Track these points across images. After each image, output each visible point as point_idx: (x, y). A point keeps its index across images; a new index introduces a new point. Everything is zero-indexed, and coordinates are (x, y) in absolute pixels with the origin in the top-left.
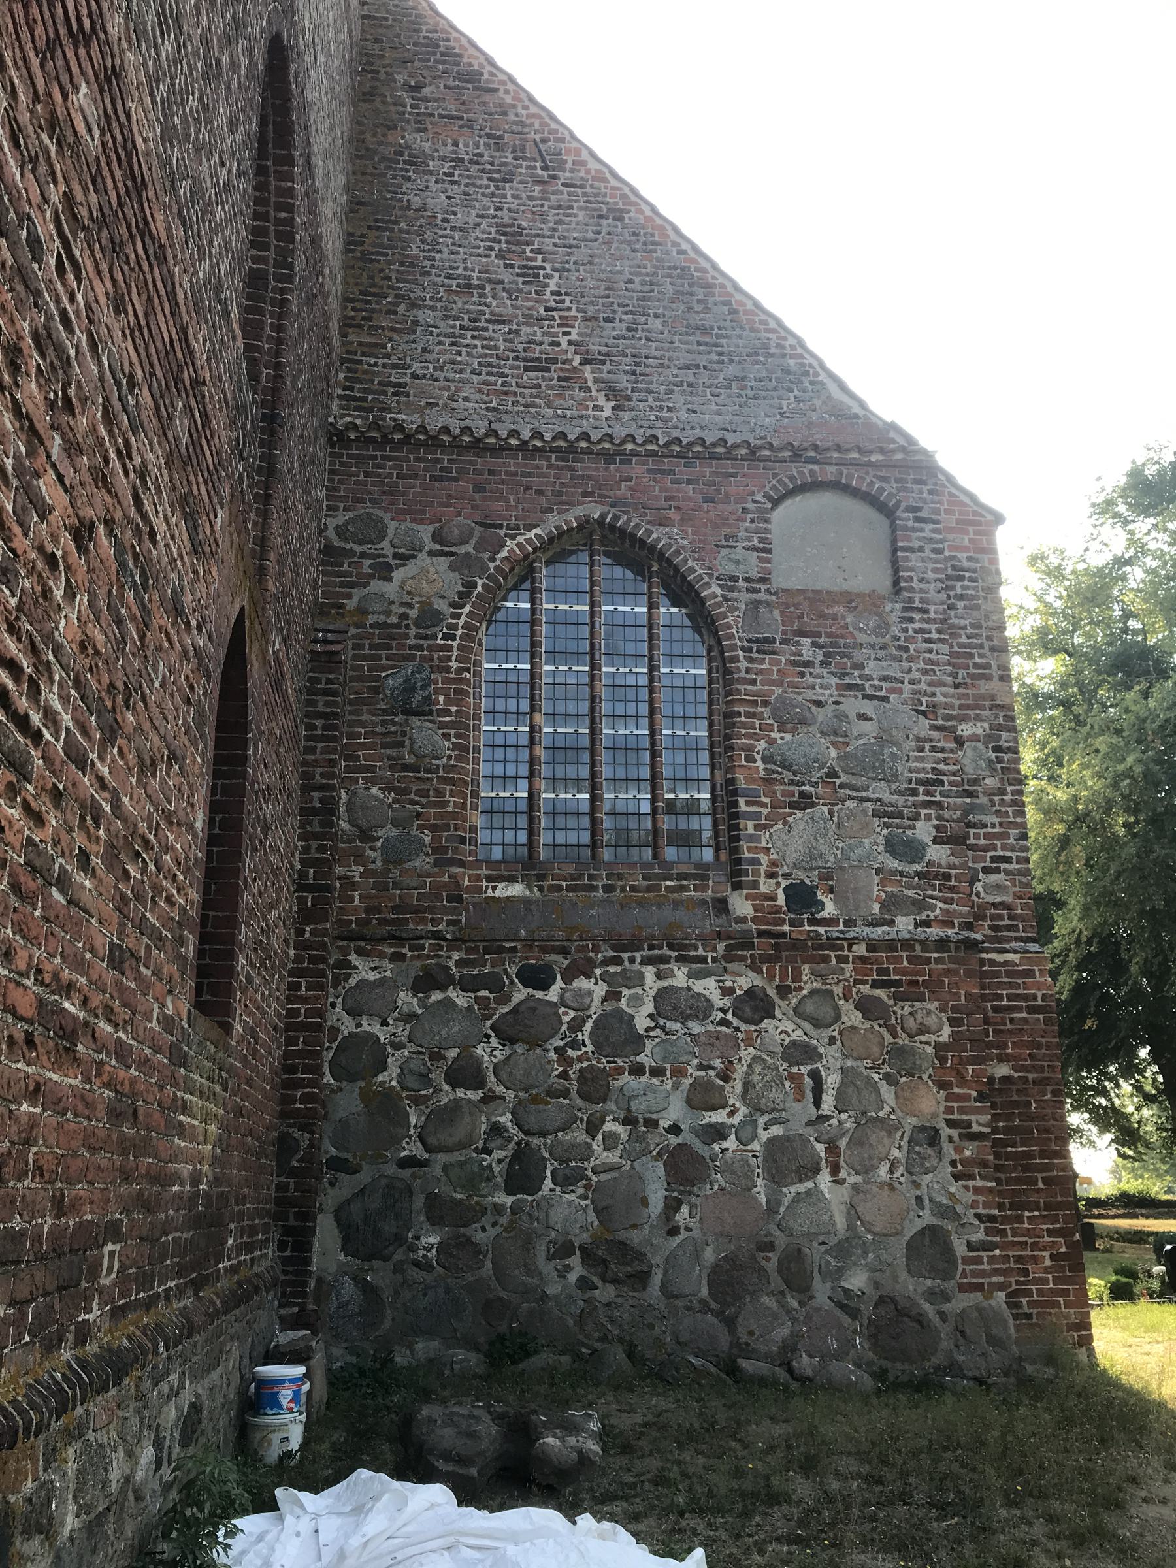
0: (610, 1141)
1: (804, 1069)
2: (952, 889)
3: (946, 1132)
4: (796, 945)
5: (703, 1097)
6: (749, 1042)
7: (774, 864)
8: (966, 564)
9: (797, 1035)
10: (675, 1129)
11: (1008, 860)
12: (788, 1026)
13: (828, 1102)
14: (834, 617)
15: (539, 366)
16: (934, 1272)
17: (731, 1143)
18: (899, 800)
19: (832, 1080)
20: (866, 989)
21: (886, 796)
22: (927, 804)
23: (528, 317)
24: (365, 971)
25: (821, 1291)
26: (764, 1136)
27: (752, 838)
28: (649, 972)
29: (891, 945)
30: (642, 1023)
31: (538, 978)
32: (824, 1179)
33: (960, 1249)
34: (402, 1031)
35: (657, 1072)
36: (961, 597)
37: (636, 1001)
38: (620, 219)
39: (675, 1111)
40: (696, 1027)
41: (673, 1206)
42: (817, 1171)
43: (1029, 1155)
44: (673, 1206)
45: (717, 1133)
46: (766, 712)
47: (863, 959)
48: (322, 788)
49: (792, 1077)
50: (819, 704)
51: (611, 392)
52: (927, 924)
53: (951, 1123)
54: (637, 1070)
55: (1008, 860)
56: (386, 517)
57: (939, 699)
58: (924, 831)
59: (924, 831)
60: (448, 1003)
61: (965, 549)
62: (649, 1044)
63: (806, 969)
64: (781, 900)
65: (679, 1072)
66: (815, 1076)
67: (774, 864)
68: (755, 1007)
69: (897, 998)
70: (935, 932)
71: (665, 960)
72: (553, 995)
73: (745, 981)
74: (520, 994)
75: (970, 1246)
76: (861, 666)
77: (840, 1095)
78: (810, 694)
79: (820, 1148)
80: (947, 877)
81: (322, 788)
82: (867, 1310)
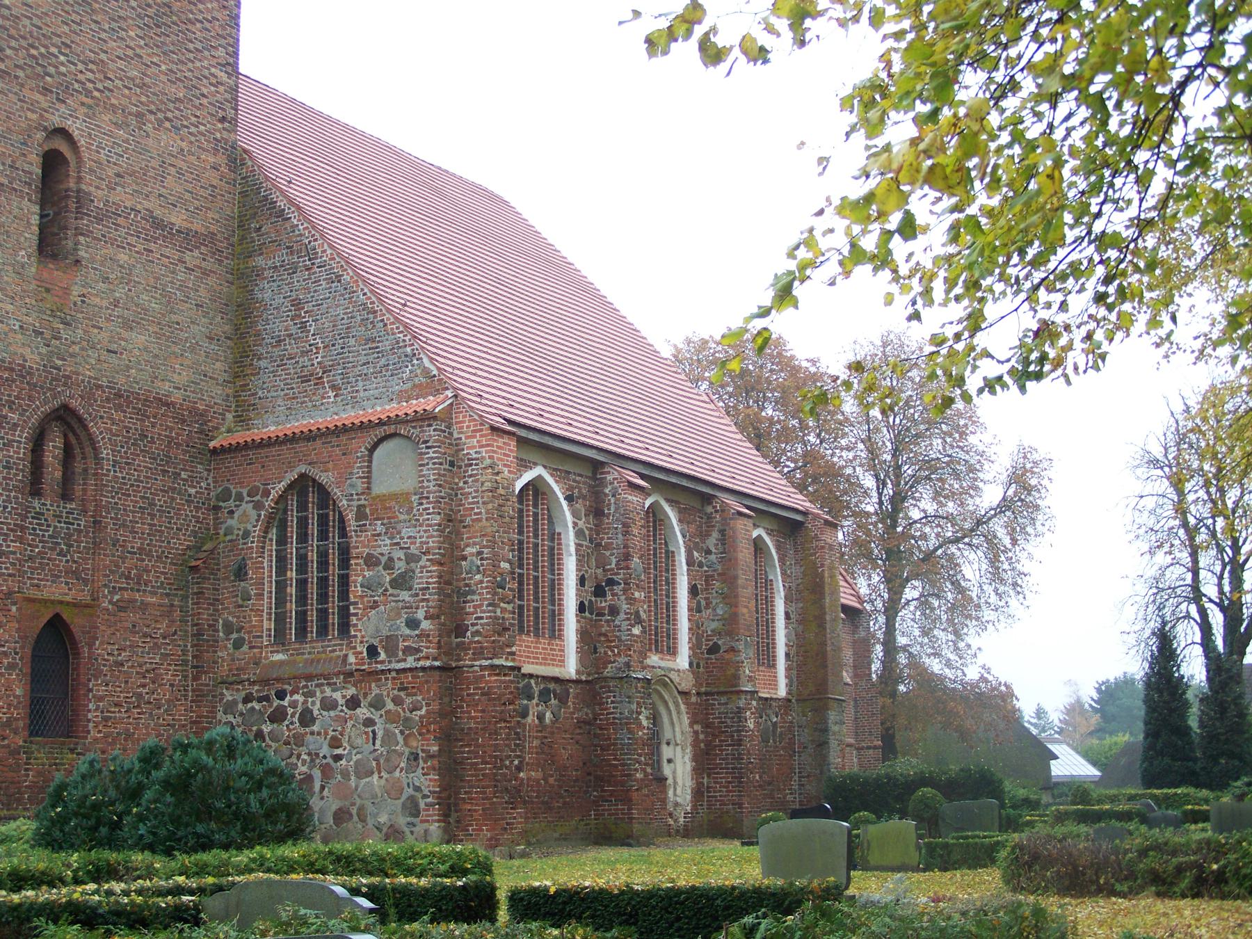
0: (304, 762)
1: (370, 729)
2: (430, 642)
3: (421, 754)
4: (370, 673)
5: (335, 743)
6: (351, 718)
7: (363, 637)
8: (475, 456)
9: (368, 715)
10: (325, 757)
11: (481, 618)
12: (365, 711)
13: (378, 742)
14: (390, 508)
15: (305, 379)
16: (412, 815)
17: (343, 762)
18: (411, 599)
19: (380, 734)
20: (396, 692)
21: (407, 599)
22: (423, 600)
23: (302, 352)
24: (228, 696)
25: (370, 821)
26: (354, 758)
27: (356, 625)
28: (318, 690)
29: (404, 670)
30: (316, 712)
31: (281, 695)
32: (376, 776)
33: (422, 806)
34: (240, 720)
35: (319, 734)
36: (471, 476)
37: (313, 703)
38: (339, 281)
39: (325, 750)
40: (332, 713)
41: (323, 788)
42: (373, 773)
43: (476, 764)
44: (323, 788)
45: (337, 758)
46: (361, 561)
47: (394, 678)
48: (197, 625)
49: (366, 733)
50: (382, 554)
51: (333, 387)
52: (419, 659)
53: (423, 751)
54: (312, 733)
55: (481, 618)
56: (232, 487)
57: (431, 544)
58: (420, 614)
59: (420, 614)
60: (253, 708)
61: (474, 447)
62: (317, 722)
63: (373, 685)
64: (365, 654)
65: (326, 733)
66: (374, 732)
67: (363, 637)
68: (353, 703)
69: (407, 695)
70: (421, 663)
71: (322, 685)
72: (286, 703)
73: (352, 691)
74: (276, 702)
75: (426, 804)
76: (399, 533)
77: (383, 740)
78: (379, 550)
79: (374, 764)
80: (428, 636)
81: (197, 625)
82: (385, 830)
